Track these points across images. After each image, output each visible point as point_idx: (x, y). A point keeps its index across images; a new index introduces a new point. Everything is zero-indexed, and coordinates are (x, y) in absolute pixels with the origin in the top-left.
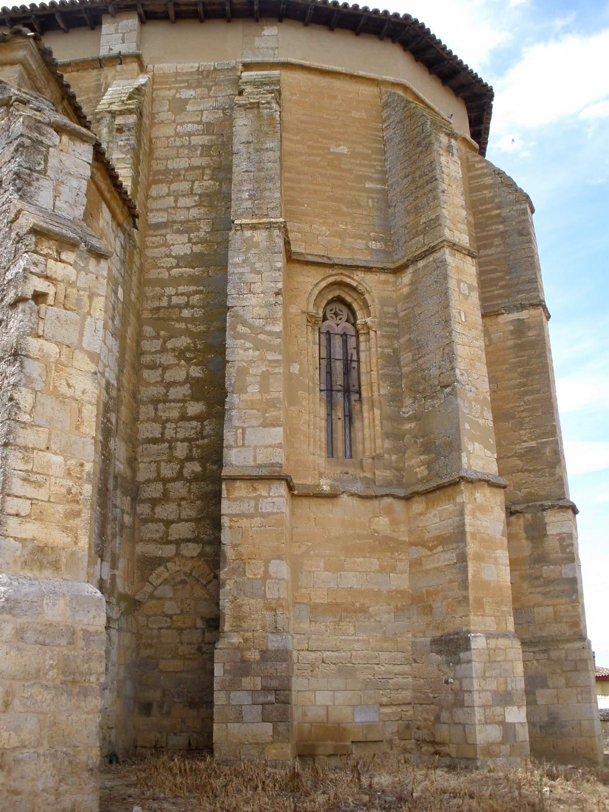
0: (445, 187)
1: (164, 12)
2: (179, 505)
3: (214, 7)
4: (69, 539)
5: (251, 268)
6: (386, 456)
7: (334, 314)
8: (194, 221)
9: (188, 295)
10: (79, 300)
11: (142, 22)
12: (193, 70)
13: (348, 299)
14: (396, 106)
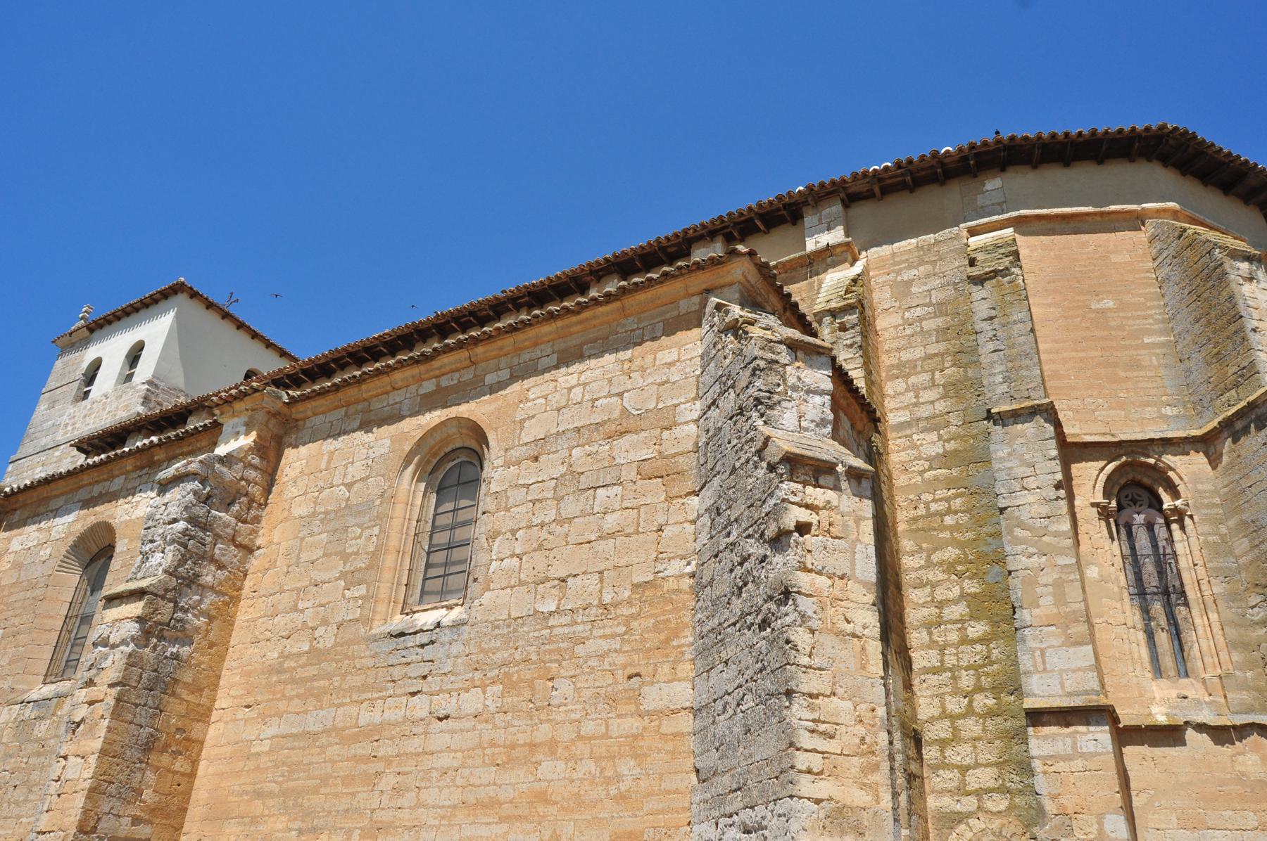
0: (1255, 324)
1: (868, 191)
2: (975, 747)
3: (924, 173)
4: (869, 798)
5: (1021, 461)
6: (1238, 673)
7: (1131, 500)
8: (941, 415)
9: (947, 500)
10: (845, 526)
11: (846, 206)
12: (912, 247)
13: (1146, 481)
14: (1168, 237)
